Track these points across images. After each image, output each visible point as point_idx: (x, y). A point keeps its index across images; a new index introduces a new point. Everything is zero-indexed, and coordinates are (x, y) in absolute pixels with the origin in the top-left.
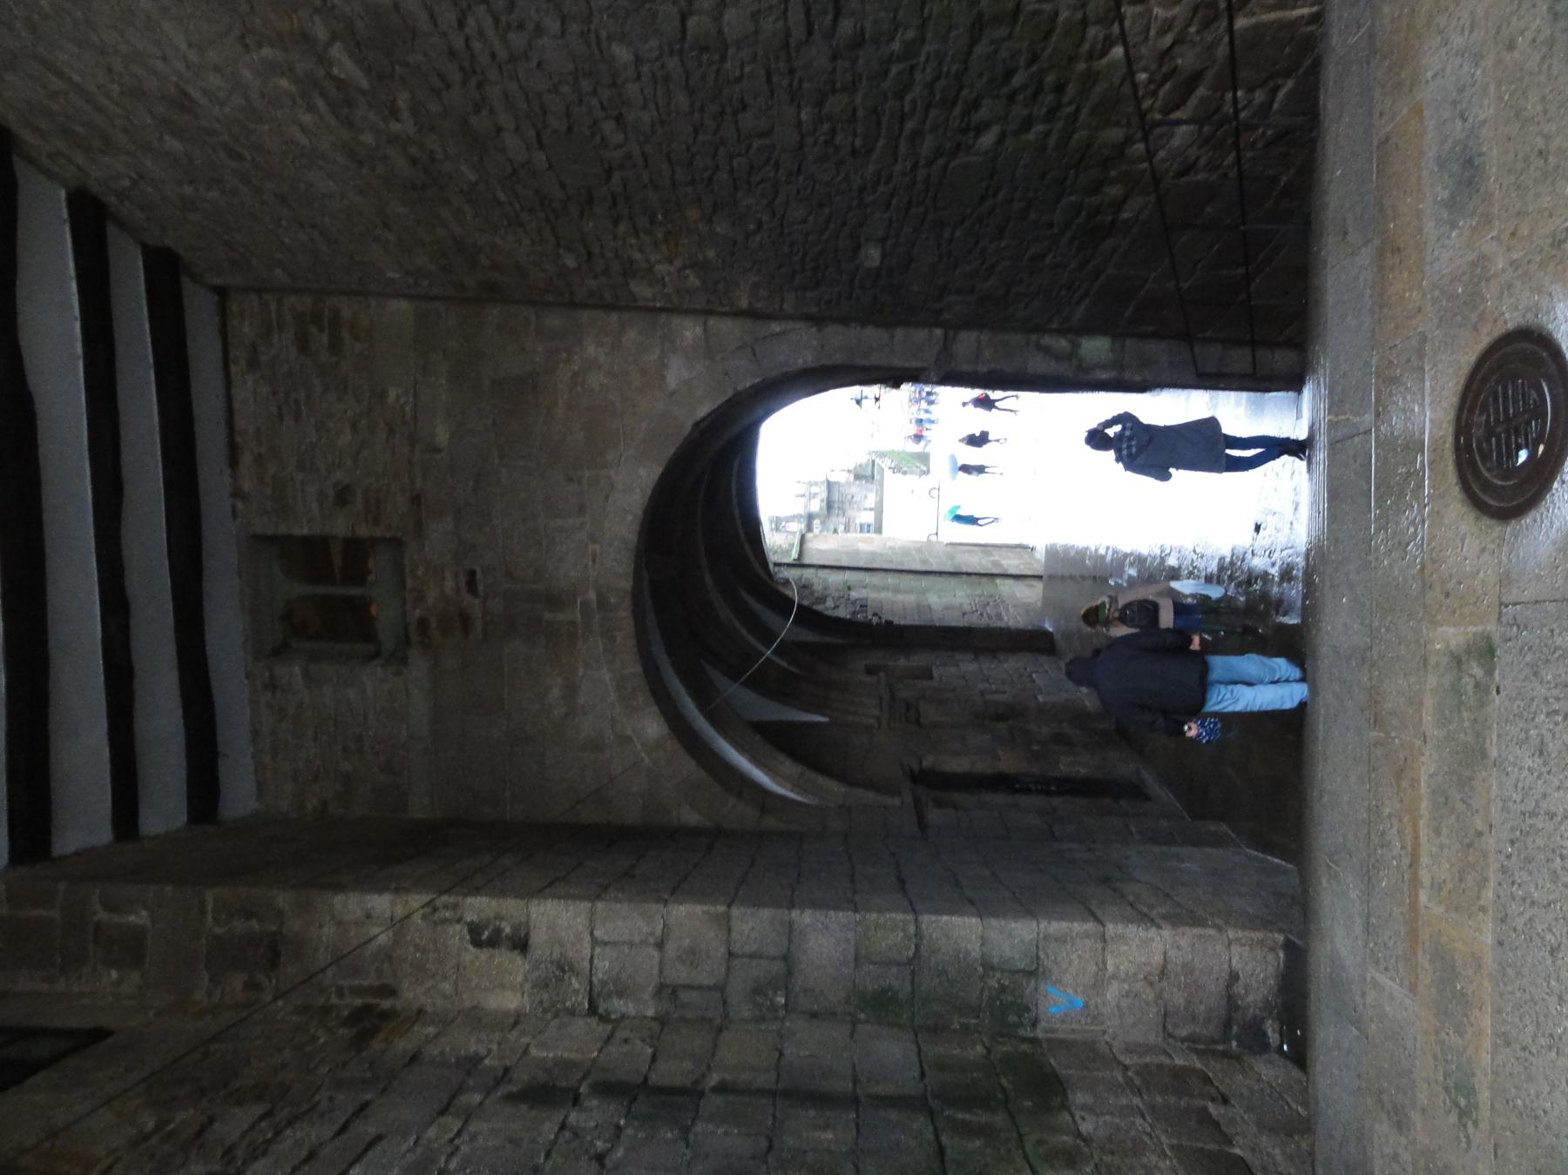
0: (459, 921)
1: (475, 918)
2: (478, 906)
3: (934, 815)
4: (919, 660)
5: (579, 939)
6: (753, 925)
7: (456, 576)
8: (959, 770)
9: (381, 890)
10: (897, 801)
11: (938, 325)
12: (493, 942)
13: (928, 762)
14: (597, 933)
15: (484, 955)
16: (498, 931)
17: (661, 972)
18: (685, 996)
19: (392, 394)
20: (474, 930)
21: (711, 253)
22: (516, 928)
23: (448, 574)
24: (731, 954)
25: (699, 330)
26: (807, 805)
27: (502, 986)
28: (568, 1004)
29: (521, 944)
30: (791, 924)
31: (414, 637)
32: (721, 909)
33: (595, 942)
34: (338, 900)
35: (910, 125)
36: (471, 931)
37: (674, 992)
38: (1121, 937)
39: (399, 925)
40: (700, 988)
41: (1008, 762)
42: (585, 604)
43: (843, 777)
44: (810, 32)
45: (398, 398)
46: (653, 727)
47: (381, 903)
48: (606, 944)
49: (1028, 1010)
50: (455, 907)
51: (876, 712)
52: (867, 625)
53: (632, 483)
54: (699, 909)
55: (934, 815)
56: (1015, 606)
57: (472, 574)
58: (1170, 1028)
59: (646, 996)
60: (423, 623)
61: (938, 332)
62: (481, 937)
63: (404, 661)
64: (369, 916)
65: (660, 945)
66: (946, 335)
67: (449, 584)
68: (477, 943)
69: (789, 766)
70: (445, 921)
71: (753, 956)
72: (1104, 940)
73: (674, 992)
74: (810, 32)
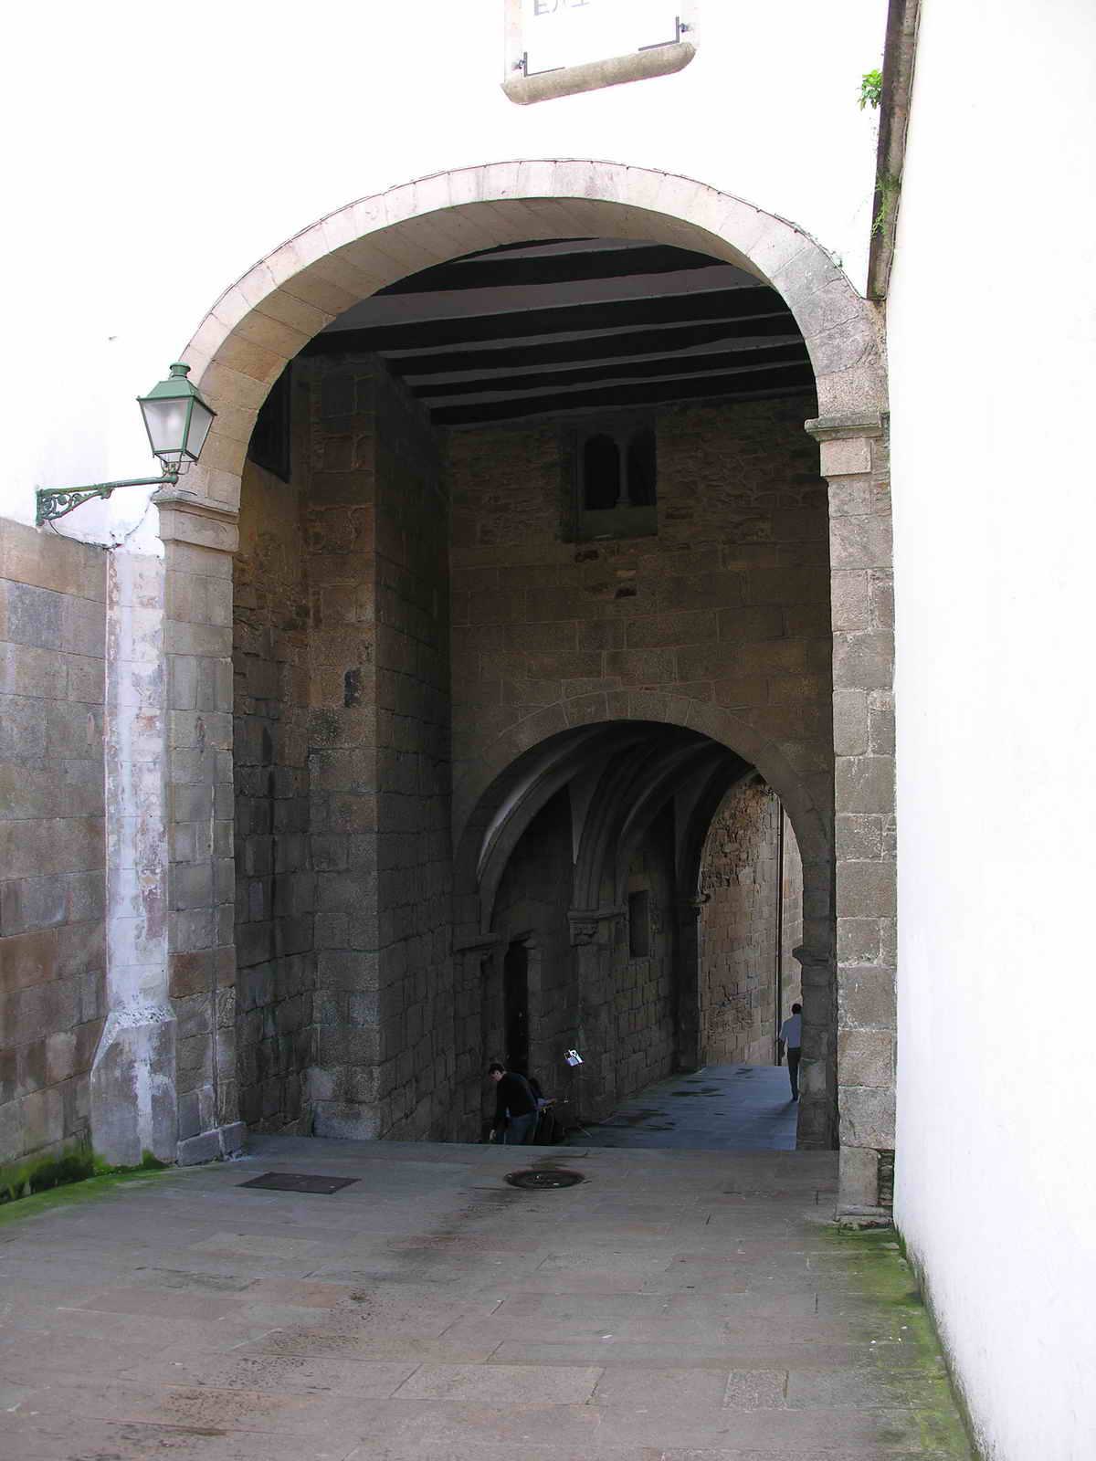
1: (362, 674)
2: (369, 672)
3: (473, 960)
4: (658, 943)
6: (365, 847)
9: (377, 611)
12: (348, 684)
15: (342, 680)
16: (356, 690)
19: (766, 526)
23: (633, 573)
26: (476, 866)
29: (350, 701)
31: (584, 548)
38: (371, 1078)
43: (503, 883)
45: (762, 530)
46: (527, 739)
47: (369, 614)
49: (737, 901)
50: (369, 660)
57: (632, 593)
62: (352, 680)
63: (567, 540)
64: (361, 606)
67: (622, 574)
68: (348, 677)
69: (509, 844)
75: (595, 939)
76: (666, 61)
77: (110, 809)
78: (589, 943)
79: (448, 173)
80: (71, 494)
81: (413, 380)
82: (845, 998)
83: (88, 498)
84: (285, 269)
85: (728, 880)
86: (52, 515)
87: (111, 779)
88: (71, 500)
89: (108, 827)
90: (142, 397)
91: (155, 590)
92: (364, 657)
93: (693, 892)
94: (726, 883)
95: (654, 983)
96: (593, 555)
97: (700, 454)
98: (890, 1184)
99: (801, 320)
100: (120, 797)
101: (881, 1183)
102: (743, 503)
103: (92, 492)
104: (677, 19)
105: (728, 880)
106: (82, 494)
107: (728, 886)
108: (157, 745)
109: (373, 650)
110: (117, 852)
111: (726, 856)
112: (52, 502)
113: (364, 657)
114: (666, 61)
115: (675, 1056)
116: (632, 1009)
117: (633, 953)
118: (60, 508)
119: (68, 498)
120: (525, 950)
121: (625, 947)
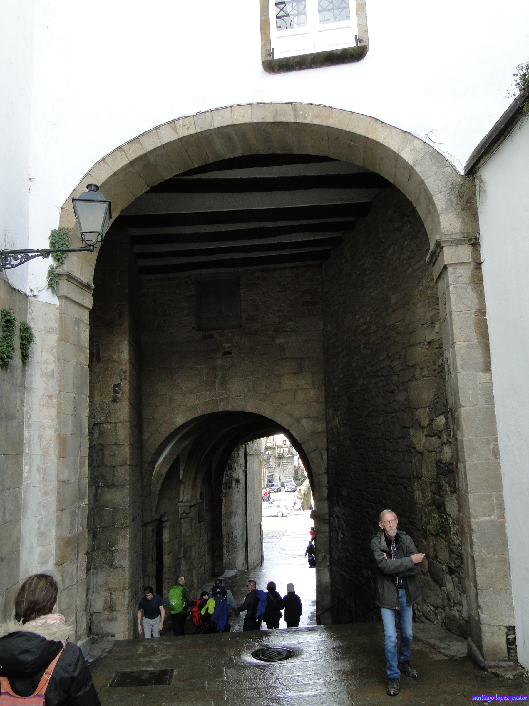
0: (121, 380)
1: (122, 385)
3: (149, 528)
5: (117, 418)
7: (230, 347)
8: (164, 537)
10: (154, 513)
11: (329, 517)
12: (115, 391)
13: (167, 524)
14: (119, 424)
17: (107, 445)
18: (100, 453)
19: (291, 324)
20: (118, 385)
21: (342, 437)
22: (119, 398)
23: (229, 345)
24: (114, 467)
25: (321, 430)
27: (101, 395)
28: (96, 417)
30: (125, 485)
32: (128, 463)
33: (116, 423)
34: (126, 343)
35: (374, 505)
36: (118, 384)
37: (101, 450)
38: (124, 596)
39: (119, 362)
40: (103, 458)
41: (167, 559)
42: (223, 394)
43: (162, 490)
44: (389, 476)
46: (180, 421)
48: (116, 427)
51: (185, 500)
52: (220, 491)
53: (267, 411)
54: (128, 456)
55: (149, 528)
56: (233, 558)
57: (230, 353)
58: (96, 614)
59: (100, 441)
60: (212, 336)
61: (327, 517)
64: (122, 352)
65: (116, 444)
66: (327, 520)
67: (226, 345)
68: (114, 386)
69: (164, 471)
70: (121, 376)
71: (114, 474)
72: (123, 590)
73: (101, 450)
74: (389, 476)
75: (190, 515)
77: (26, 450)
79: (231, 107)
80: (22, 255)
81: (138, 249)
82: (477, 538)
83: (33, 257)
84: (135, 153)
86: (8, 266)
87: (27, 431)
88: (22, 258)
89: (24, 461)
90: (75, 198)
91: (54, 324)
92: (123, 377)
96: (212, 336)
97: (261, 292)
98: (514, 647)
100: (32, 442)
101: (509, 646)
103: (37, 254)
104: (356, 36)
106: (30, 255)
108: (53, 412)
109: (128, 374)
110: (28, 478)
112: (9, 258)
113: (123, 377)
114: (355, 55)
115: (213, 567)
118: (14, 262)
119: (19, 256)
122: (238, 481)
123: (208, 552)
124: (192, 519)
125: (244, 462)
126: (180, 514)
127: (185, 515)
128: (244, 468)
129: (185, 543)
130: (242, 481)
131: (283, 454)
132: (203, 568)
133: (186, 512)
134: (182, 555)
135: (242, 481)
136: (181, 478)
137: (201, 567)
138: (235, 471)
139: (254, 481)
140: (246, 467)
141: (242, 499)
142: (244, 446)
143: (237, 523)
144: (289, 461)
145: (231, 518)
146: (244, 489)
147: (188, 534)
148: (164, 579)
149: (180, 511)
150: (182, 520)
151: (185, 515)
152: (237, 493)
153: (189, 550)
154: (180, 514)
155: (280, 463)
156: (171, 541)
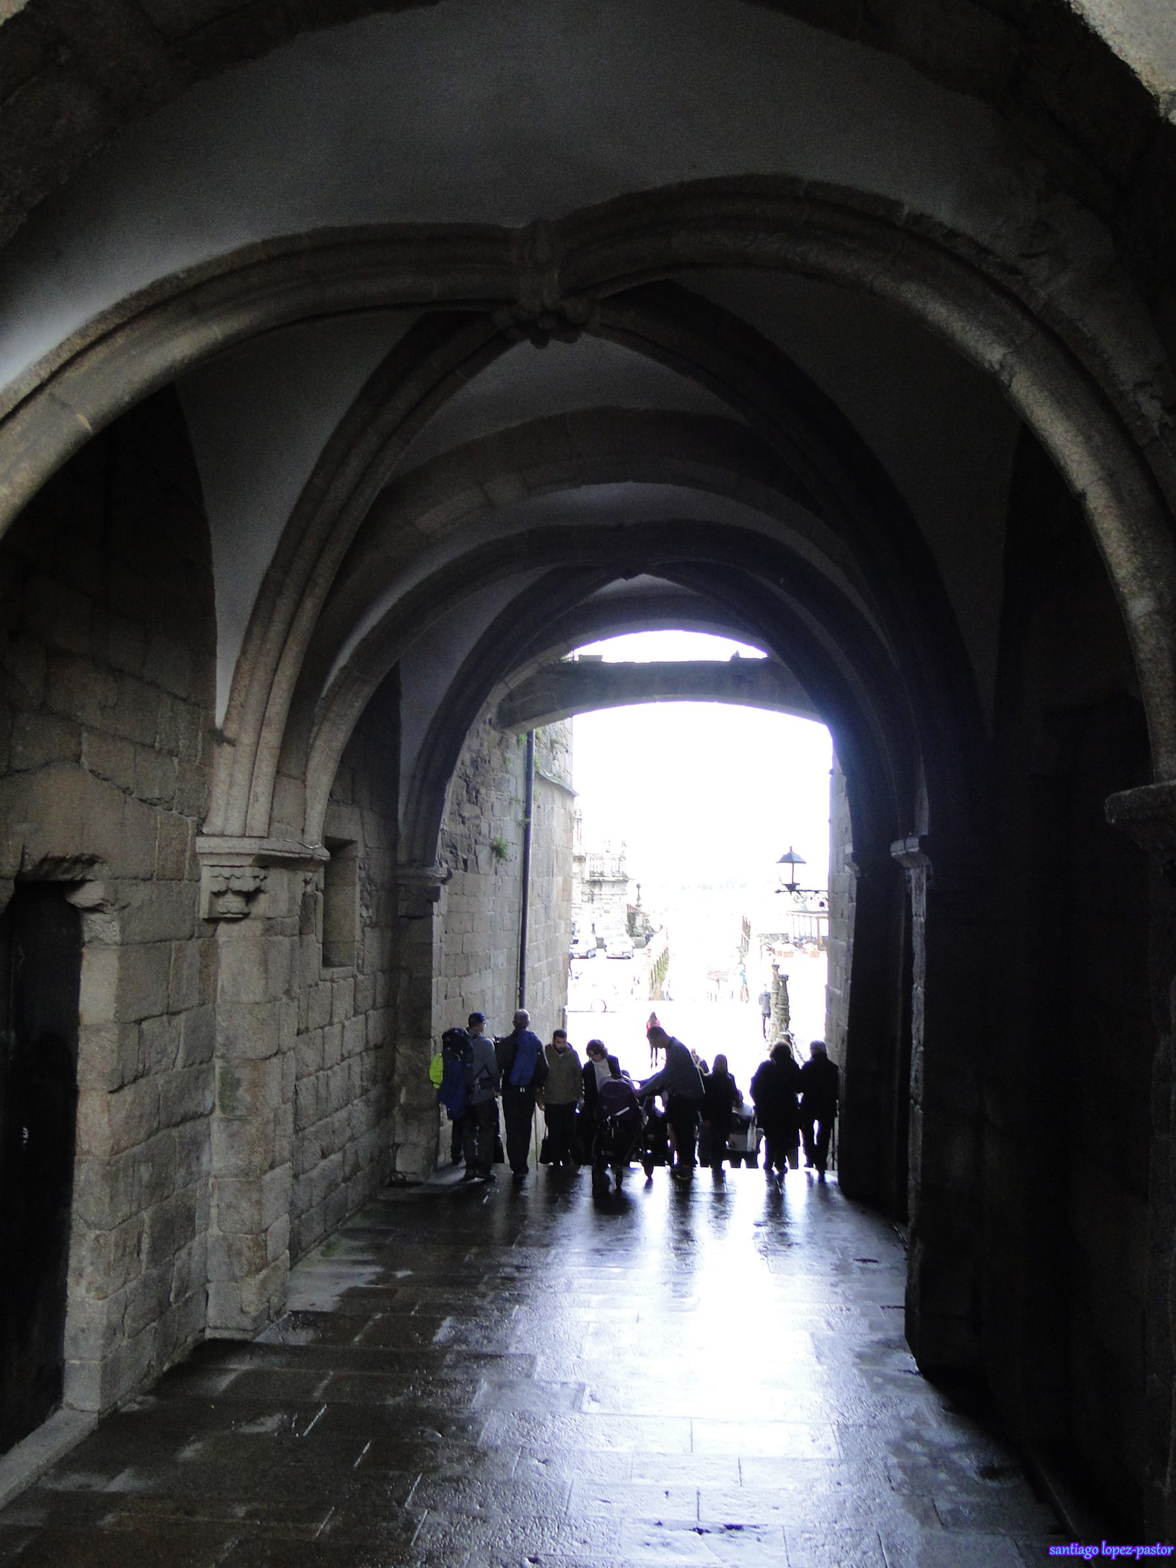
4: (365, 944)
75: (261, 906)
76: (746, 927)
78: (246, 916)
85: (465, 861)
93: (427, 858)
94: (461, 865)
95: (362, 1017)
99: (534, 855)
102: (276, 1224)
105: (465, 861)
107: (465, 871)
111: (463, 823)
116: (322, 1069)
117: (327, 962)
120: (76, 915)
121: (314, 942)
122: (498, 851)
123: (365, 1091)
124: (270, 926)
125: (521, 796)
126: (205, 898)
127: (233, 904)
128: (520, 816)
129: (229, 1042)
130: (514, 851)
131: (602, 874)
132: (336, 1157)
133: (237, 885)
134: (211, 1097)
135: (514, 851)
136: (219, 720)
137: (324, 1156)
138: (488, 814)
139: (550, 873)
140: (527, 813)
141: (510, 919)
142: (524, 738)
143: (488, 997)
144: (616, 890)
145: (468, 974)
146: (519, 885)
147: (247, 998)
148: (78, 1226)
149: (208, 881)
150: (222, 927)
151: (233, 904)
152: (493, 892)
153: (245, 1074)
154: (205, 898)
155: (593, 895)
156: (131, 1023)
